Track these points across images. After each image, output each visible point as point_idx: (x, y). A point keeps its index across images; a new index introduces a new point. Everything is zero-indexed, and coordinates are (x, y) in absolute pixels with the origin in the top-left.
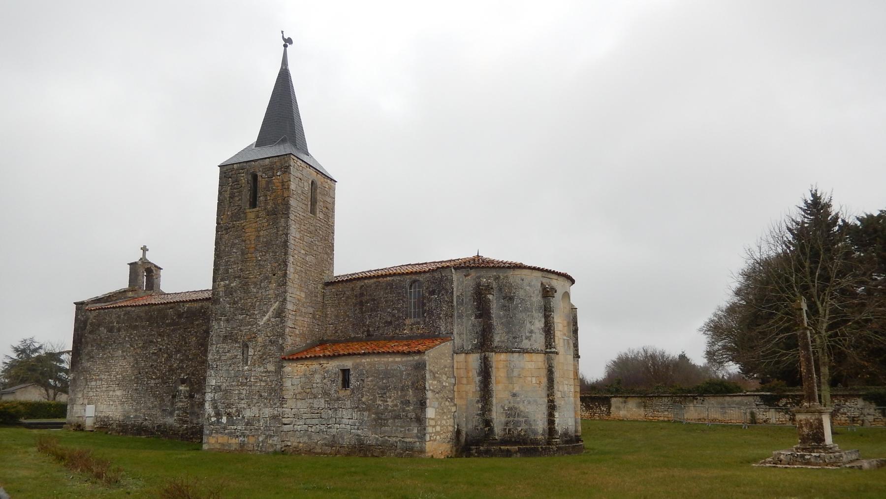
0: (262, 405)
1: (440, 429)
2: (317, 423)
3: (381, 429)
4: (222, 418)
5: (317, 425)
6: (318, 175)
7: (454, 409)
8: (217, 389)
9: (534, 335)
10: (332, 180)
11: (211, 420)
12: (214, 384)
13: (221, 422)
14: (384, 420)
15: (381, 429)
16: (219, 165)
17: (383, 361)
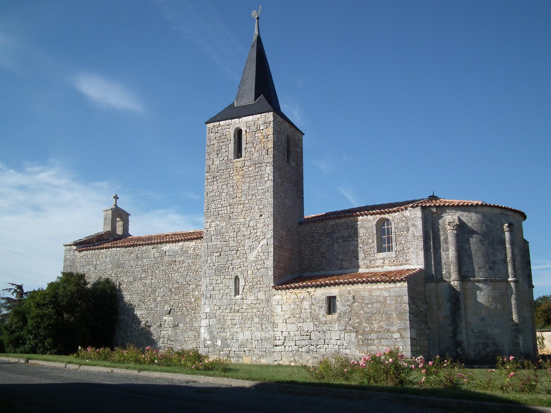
0: (255, 329)
1: (420, 349)
2: (307, 344)
3: (368, 348)
4: (216, 342)
5: (307, 345)
6: (291, 129)
7: (428, 332)
8: (209, 316)
9: (496, 266)
10: (300, 132)
11: (207, 343)
12: (208, 311)
13: (217, 345)
14: (371, 340)
15: (368, 348)
16: (205, 122)
17: (367, 288)
